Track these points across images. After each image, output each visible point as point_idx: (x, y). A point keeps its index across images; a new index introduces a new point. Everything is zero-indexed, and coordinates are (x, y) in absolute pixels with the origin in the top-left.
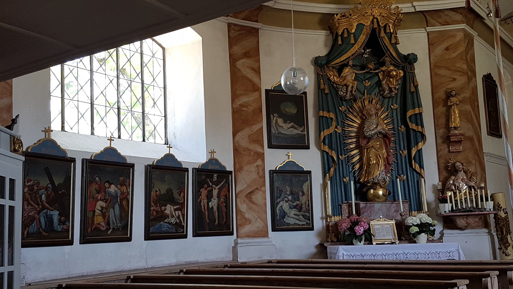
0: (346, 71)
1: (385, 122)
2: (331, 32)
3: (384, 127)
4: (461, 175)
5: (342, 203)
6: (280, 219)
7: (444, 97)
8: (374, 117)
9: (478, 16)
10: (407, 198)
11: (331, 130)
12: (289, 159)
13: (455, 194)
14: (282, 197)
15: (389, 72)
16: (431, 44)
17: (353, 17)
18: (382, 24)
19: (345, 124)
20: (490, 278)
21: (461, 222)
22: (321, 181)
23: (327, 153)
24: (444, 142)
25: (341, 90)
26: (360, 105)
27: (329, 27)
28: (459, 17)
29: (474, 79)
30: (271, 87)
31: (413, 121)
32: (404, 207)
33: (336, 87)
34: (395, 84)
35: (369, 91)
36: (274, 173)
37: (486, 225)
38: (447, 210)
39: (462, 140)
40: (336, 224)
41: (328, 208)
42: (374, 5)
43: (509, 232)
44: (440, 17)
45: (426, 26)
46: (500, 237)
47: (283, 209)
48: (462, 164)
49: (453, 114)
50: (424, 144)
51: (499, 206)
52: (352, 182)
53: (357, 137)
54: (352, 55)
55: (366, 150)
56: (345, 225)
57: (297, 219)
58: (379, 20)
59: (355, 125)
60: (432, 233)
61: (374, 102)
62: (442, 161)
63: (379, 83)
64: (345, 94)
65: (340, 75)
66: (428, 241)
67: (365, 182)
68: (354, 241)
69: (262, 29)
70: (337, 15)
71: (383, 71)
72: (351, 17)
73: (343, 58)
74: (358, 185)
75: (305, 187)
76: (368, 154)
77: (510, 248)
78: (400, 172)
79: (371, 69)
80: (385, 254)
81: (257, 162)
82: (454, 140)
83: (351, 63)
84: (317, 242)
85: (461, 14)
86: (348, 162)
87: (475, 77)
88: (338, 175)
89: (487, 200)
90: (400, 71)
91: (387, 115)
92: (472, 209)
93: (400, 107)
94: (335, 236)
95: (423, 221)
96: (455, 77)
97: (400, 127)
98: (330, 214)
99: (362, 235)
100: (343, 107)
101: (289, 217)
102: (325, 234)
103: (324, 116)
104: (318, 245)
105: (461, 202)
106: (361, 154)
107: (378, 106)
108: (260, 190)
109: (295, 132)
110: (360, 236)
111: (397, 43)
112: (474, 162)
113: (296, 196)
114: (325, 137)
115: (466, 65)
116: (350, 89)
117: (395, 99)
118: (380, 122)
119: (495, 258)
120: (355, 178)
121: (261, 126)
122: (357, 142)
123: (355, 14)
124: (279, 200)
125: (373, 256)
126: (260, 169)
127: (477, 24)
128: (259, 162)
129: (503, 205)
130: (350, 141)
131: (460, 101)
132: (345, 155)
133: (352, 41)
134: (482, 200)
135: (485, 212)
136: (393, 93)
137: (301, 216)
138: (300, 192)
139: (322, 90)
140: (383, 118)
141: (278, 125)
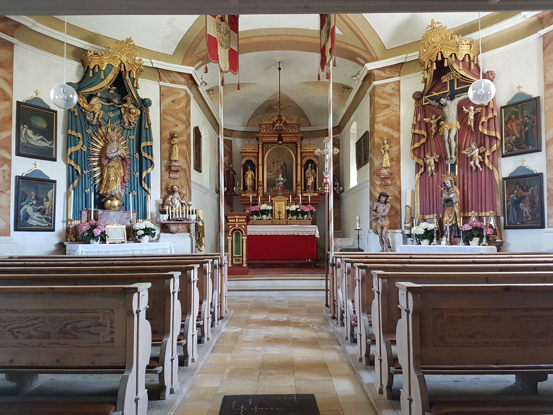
0: (95, 100)
1: (124, 148)
2: (83, 64)
3: (122, 152)
4: (177, 195)
5: (82, 209)
6: (23, 220)
7: (169, 137)
8: (115, 143)
9: (195, 83)
10: (136, 209)
11: (78, 148)
12: (35, 168)
13: (172, 208)
14: (27, 201)
15: (130, 109)
16: (162, 95)
17: (104, 57)
18: (128, 69)
19: (90, 145)
20: (173, 279)
21: (173, 228)
22: (65, 190)
23: (73, 167)
24: (166, 170)
25: (89, 116)
26: (104, 131)
27: (81, 60)
28: (183, 80)
29: (189, 128)
30: (23, 99)
31: (146, 151)
32: (133, 216)
33: (85, 112)
34: (134, 119)
35: (112, 120)
36: (20, 178)
37: (189, 231)
38: (165, 219)
39: (179, 170)
40: (76, 228)
41: (70, 213)
42: (123, 52)
43: (203, 236)
44: (170, 76)
45: (159, 80)
46: (197, 239)
47: (27, 212)
48: (178, 187)
49: (174, 150)
50: (152, 170)
51: (199, 218)
52: (93, 194)
53: (100, 157)
54: (101, 89)
55: (106, 168)
56: (85, 228)
57: (39, 221)
58: (126, 66)
59: (98, 146)
60: (153, 235)
61: (116, 130)
62: (164, 184)
63: (121, 116)
64: (92, 119)
65: (88, 103)
66: (149, 241)
67: (104, 194)
68: (91, 241)
69: (17, 45)
70: (90, 52)
71: (125, 107)
72: (103, 56)
73: (92, 89)
74: (97, 196)
75: (50, 194)
76: (108, 171)
77: (203, 247)
78: (133, 189)
79: (115, 103)
80: (117, 251)
81: (3, 167)
82: (174, 169)
83: (99, 95)
84: (57, 241)
85: (184, 78)
86: (91, 176)
87: (190, 127)
88: (80, 186)
89: (193, 214)
90: (138, 110)
91: (126, 143)
92: (182, 219)
93: (136, 138)
94: (74, 237)
95: (147, 227)
96: (178, 124)
97: (135, 154)
98: (72, 218)
99: (99, 236)
100: (89, 130)
101: (32, 219)
102: (65, 234)
103: (73, 134)
104: (58, 243)
105: (176, 214)
106: (102, 171)
107: (119, 134)
108: (4, 193)
109: (44, 144)
110: (97, 236)
111: (137, 88)
112: (185, 186)
113: (40, 201)
114: (71, 153)
115: (185, 117)
116: (96, 116)
117: (132, 130)
118: (120, 147)
119: (192, 252)
120: (95, 190)
121: (10, 134)
122: (100, 161)
123: (107, 55)
124: (23, 203)
125: (107, 253)
126: (6, 174)
127: (193, 88)
128: (6, 167)
129: (201, 218)
130: (93, 159)
131: (180, 142)
132: (88, 170)
133: (102, 77)
134: (189, 214)
135: (191, 222)
136: (132, 127)
137: (44, 219)
138: (45, 198)
139: (71, 112)
140: (122, 145)
141: (28, 136)
